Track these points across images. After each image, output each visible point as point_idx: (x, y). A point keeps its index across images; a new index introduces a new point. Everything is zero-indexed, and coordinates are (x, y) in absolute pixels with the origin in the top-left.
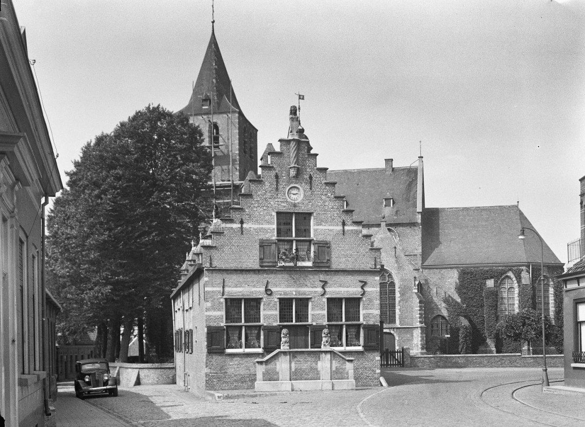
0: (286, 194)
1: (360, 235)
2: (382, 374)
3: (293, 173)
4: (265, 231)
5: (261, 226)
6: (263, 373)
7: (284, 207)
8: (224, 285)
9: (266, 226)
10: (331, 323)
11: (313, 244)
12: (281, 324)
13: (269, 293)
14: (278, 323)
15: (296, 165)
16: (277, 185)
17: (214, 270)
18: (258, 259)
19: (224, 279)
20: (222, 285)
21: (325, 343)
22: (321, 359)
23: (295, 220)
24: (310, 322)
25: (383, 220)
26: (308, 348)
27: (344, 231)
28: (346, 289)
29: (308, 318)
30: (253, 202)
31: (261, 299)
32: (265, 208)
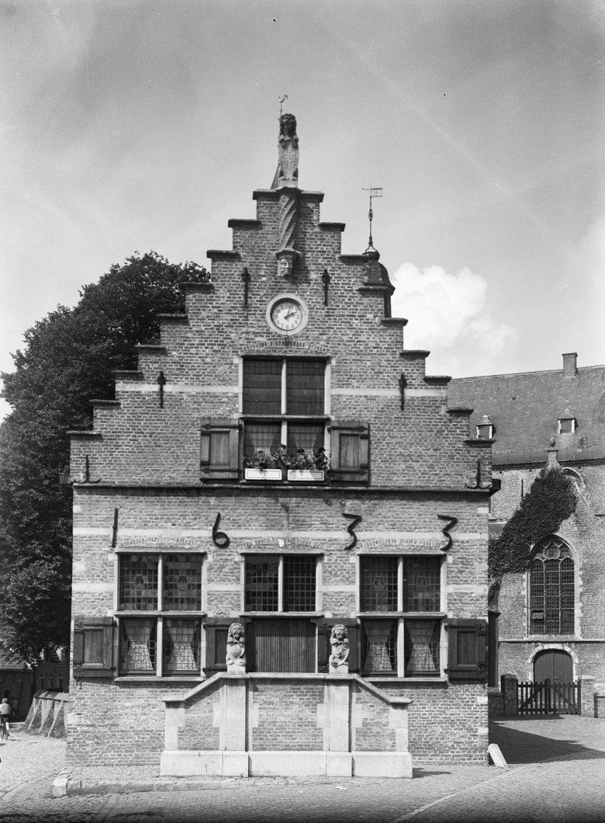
0: (268, 316)
1: (443, 410)
2: (492, 738)
3: (283, 267)
4: (215, 399)
5: (207, 389)
6: (181, 732)
7: (262, 345)
8: (116, 523)
9: (218, 389)
10: (368, 614)
11: (329, 430)
13: (221, 541)
14: (242, 613)
15: (290, 249)
16: (246, 296)
17: (94, 487)
18: (198, 465)
19: (117, 510)
20: (113, 522)
21: (337, 660)
22: (326, 699)
23: (288, 375)
24: (318, 612)
25: (552, 449)
26: (314, 672)
27: (402, 400)
28: (405, 535)
29: (314, 602)
30: (190, 335)
31: (204, 555)
32: (216, 348)
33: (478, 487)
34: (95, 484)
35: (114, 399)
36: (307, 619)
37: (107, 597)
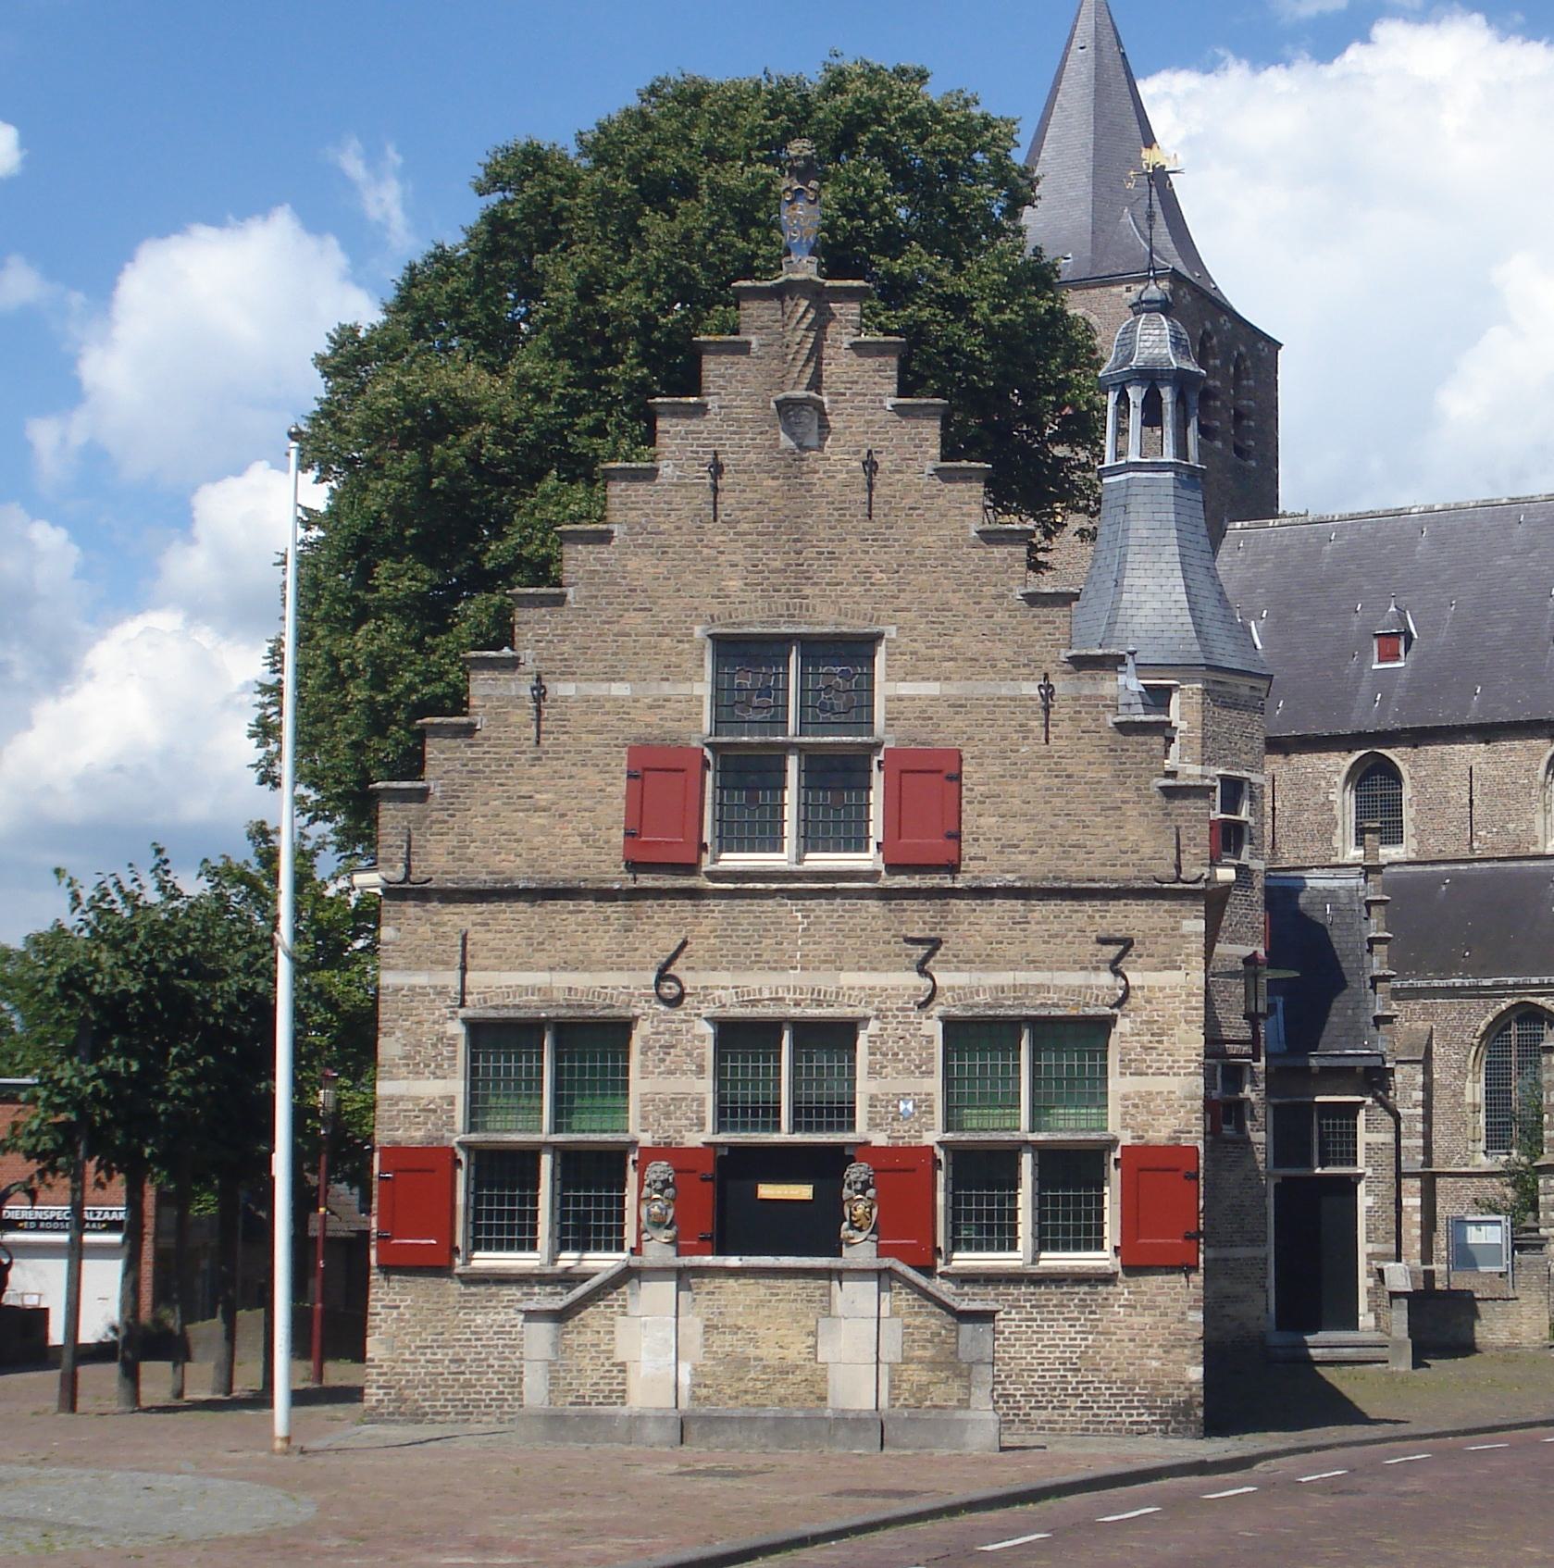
12: (723, 1137)
33: (406, 879)
34: (1190, 886)
35: (465, 714)
36: (838, 1149)
37: (923, 1105)
